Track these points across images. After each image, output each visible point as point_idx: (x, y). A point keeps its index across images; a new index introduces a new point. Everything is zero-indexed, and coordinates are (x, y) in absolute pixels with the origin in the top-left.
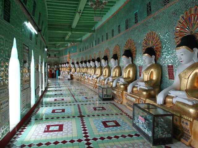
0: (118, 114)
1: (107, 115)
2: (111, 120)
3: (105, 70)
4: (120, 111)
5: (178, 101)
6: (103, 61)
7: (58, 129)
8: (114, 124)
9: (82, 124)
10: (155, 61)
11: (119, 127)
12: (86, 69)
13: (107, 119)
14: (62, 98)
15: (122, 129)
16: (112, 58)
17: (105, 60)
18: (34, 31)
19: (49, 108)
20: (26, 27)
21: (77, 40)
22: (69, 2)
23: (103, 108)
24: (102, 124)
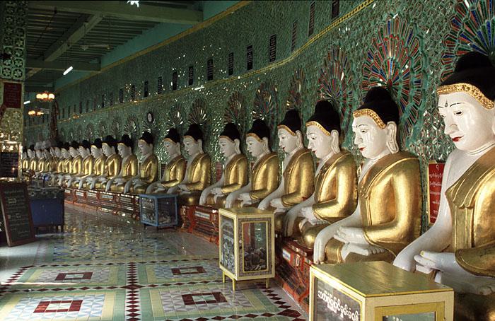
3: (233, 170)
6: (189, 142)
10: (399, 140)
16: (223, 134)
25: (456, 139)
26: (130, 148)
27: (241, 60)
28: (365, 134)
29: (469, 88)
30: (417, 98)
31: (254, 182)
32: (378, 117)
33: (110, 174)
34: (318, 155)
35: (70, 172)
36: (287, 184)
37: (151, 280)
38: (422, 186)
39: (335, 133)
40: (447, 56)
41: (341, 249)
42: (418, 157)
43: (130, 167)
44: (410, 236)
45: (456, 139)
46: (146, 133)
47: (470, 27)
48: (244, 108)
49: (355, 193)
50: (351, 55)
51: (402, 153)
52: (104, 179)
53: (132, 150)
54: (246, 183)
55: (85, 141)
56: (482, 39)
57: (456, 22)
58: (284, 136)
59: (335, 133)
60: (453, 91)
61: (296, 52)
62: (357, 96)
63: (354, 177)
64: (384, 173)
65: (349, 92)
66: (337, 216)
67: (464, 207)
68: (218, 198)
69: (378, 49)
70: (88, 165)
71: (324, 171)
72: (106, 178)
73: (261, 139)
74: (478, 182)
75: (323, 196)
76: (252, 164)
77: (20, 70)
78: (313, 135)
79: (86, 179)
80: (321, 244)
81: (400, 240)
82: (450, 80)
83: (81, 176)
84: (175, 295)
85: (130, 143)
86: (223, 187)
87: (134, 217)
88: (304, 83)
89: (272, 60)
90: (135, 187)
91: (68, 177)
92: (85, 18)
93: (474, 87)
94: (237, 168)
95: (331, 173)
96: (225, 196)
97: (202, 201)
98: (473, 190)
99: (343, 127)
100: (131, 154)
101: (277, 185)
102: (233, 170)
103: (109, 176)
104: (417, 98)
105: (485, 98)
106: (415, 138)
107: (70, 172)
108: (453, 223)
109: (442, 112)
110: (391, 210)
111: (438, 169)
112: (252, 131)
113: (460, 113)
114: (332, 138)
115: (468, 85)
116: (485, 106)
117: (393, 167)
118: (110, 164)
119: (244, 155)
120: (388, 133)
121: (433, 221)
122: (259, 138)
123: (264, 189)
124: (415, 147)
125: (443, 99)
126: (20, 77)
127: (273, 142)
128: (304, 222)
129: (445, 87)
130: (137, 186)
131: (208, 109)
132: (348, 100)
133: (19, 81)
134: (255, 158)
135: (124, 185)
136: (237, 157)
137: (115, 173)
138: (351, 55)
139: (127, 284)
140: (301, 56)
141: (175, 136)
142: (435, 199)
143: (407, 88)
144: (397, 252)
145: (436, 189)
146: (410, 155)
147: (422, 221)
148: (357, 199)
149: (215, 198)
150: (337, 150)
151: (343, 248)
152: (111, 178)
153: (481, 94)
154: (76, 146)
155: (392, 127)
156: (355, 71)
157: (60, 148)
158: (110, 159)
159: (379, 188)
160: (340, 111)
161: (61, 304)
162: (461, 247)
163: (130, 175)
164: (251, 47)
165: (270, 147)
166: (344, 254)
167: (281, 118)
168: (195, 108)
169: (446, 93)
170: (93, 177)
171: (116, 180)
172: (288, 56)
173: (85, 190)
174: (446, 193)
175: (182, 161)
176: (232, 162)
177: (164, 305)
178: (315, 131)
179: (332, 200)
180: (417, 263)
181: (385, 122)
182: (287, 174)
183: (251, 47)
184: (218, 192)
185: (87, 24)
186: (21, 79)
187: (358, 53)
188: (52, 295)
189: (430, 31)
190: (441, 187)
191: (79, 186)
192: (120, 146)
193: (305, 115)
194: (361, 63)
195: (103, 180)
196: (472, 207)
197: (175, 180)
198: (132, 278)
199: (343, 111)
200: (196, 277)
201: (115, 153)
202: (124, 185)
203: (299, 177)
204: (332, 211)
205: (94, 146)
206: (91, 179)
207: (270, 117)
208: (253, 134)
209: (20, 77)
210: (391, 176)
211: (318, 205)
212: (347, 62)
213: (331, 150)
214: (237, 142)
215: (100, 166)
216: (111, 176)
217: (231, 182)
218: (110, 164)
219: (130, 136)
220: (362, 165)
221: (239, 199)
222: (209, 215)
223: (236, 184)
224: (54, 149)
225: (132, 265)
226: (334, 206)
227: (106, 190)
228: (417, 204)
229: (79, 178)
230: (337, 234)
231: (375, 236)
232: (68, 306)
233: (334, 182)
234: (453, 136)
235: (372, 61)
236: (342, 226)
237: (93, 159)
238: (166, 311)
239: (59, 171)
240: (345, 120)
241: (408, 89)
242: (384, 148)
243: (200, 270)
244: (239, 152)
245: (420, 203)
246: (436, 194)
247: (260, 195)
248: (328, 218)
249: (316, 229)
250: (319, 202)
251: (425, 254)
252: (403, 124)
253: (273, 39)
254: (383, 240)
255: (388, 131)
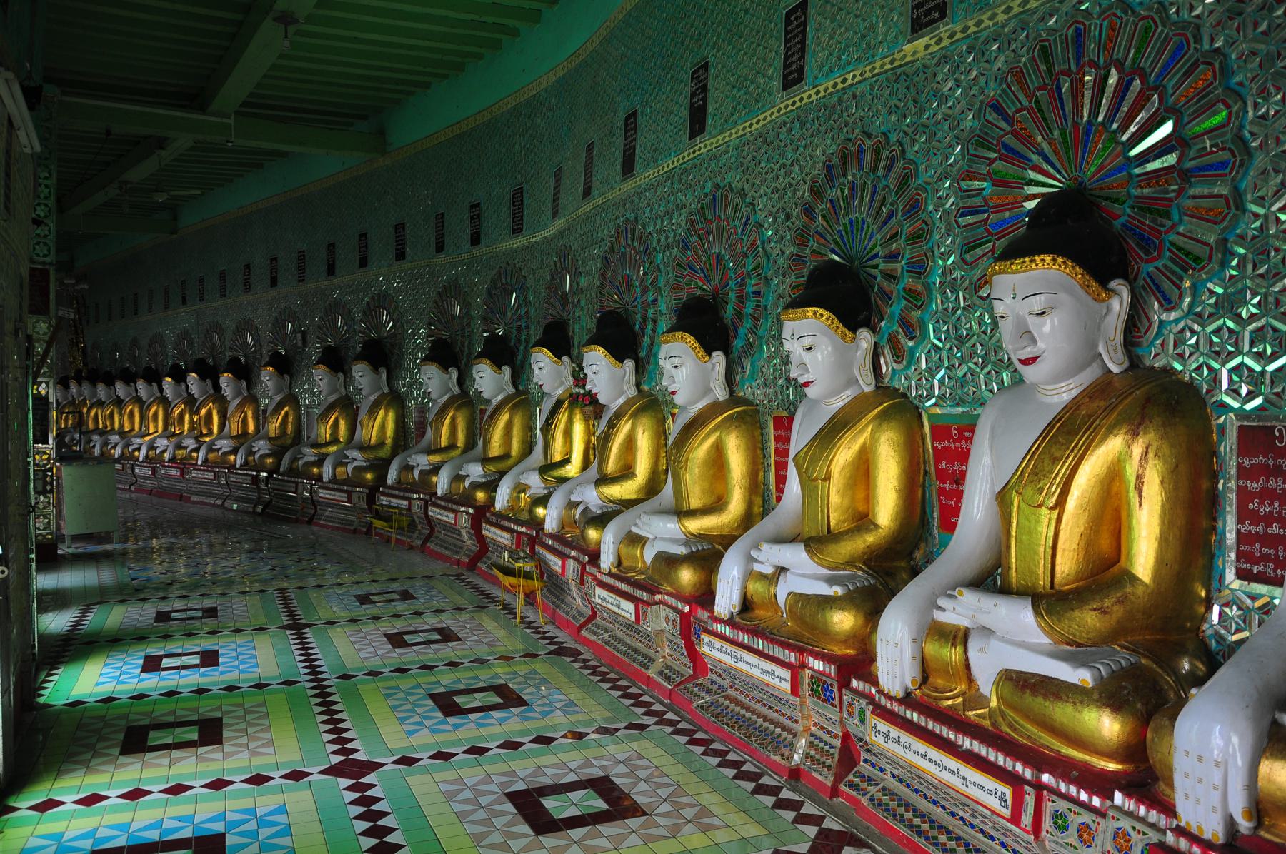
0: (535, 656)
1: (539, 740)
2: (481, 685)
3: (447, 421)
4: (628, 702)
5: (773, 513)
6: (361, 373)
7: (152, 734)
8: (600, 804)
9: (365, 825)
10: (730, 380)
11: (634, 823)
12: (342, 424)
13: (436, 651)
14: (207, 603)
15: (536, 715)
17: (375, 367)
18: (1083, 8)
19: (120, 687)
20: (1160, 561)
21: (1147, 387)
22: (408, 8)
23: (500, 690)
24: (509, 807)
25: (806, 384)
26: (244, 383)
27: (458, 226)
28: (679, 370)
29: (822, 315)
30: (756, 319)
31: (486, 443)
32: (697, 345)
33: (205, 432)
34: (602, 399)
35: (117, 426)
36: (547, 448)
37: (325, 614)
38: (764, 449)
39: (629, 365)
40: (797, 260)
41: (643, 548)
42: (757, 405)
43: (245, 417)
44: (747, 521)
45: (806, 384)
46: (276, 355)
47: (827, 221)
48: (466, 314)
49: (663, 461)
50: (656, 239)
51: (734, 400)
52: (192, 441)
53: (249, 388)
54: (470, 445)
55: (148, 368)
56: (841, 249)
57: (809, 212)
58: (541, 365)
59: (629, 365)
60: (801, 318)
61: (560, 223)
62: (666, 307)
63: (660, 434)
64: (707, 430)
65: (651, 299)
66: (634, 497)
67: (816, 479)
68: (421, 472)
69: (698, 235)
70: (156, 414)
71: (612, 425)
72: (196, 438)
73: (500, 368)
74: (835, 445)
75: (611, 466)
76: (483, 412)
77: (45, 244)
78: (594, 368)
79: (153, 441)
80: (612, 540)
81: (732, 529)
82: (799, 303)
83: (143, 436)
84: (374, 634)
85: (245, 373)
86: (429, 452)
87: (259, 509)
88: (576, 275)
89: (517, 230)
90: (257, 456)
91: (114, 438)
92: (161, 143)
93: (829, 314)
94: (453, 419)
95: (625, 428)
96: (436, 469)
97: (392, 477)
98: (828, 456)
99: (642, 354)
100: (245, 394)
101: (528, 448)
102: (447, 421)
103: (202, 435)
104: (756, 319)
105: (844, 329)
106: (753, 377)
107: (117, 426)
108: (804, 502)
109: (787, 345)
110: (153, 637)
111: (784, 425)
112: (481, 355)
113: (810, 348)
114: (625, 371)
115: (821, 311)
116: (843, 339)
117: (722, 420)
118: (203, 412)
119: (465, 398)
120: (713, 369)
121: (779, 499)
122: (495, 368)
123: (506, 456)
124: (751, 390)
125: (789, 328)
126: (45, 256)
127: (520, 373)
128: (580, 508)
129: (791, 311)
130: (262, 452)
131: (397, 312)
132: (651, 311)
133: (44, 263)
134: (488, 402)
135: (235, 451)
136: (453, 399)
137: (215, 429)
138: (656, 239)
139: (286, 623)
140: (570, 229)
141: (335, 361)
142: (782, 467)
143: (741, 299)
144: (727, 547)
145: (782, 453)
146: (744, 401)
147: (764, 501)
148: (667, 470)
149: (416, 473)
150: (632, 392)
151: (647, 545)
152: (207, 439)
153: (837, 322)
154: (129, 379)
155: (719, 358)
156: (661, 266)
157: (94, 383)
158: (203, 404)
159: (700, 450)
160: (637, 327)
161: (183, 658)
162: (814, 534)
163: (245, 434)
164: (478, 205)
165: (515, 382)
166: (649, 554)
167: (536, 333)
168: (371, 312)
169: (792, 320)
170: (168, 438)
171: (219, 444)
172: (546, 226)
173: (154, 462)
174: (794, 459)
175: (347, 406)
176: (444, 409)
177: (360, 650)
178: (598, 362)
179: (626, 472)
180: (756, 561)
181: (709, 352)
182: (548, 428)
183: (478, 205)
184: (422, 461)
185: (163, 153)
186: (48, 260)
187: (667, 238)
188: (180, 643)
189: (775, 220)
190: (788, 449)
191: (142, 454)
192: (225, 380)
193: (577, 330)
194: (671, 254)
195: (191, 443)
196: (827, 478)
197: (335, 440)
198: (291, 613)
199: (643, 330)
200: (400, 607)
201: (212, 392)
202: (235, 451)
203: (568, 433)
204: (618, 491)
205: (169, 379)
206: (165, 442)
207: (514, 330)
208: (484, 360)
209: (45, 256)
210: (718, 434)
211: (603, 480)
212: (648, 252)
213: (622, 392)
214: (454, 373)
215: (181, 416)
216: (206, 435)
217: (444, 443)
218: (203, 412)
219: (243, 360)
220: (673, 416)
221: (460, 473)
222: (406, 503)
223: (452, 446)
224: (80, 384)
225: (282, 590)
226: (630, 482)
227: (200, 463)
228: (757, 476)
229: (139, 440)
230: (636, 525)
231: (694, 525)
232: (196, 660)
233: (630, 444)
234: (801, 380)
235: (689, 253)
236: (645, 513)
237: (164, 401)
238: (365, 658)
239: (91, 426)
240: (647, 340)
241: (743, 303)
242: (708, 390)
243: (406, 595)
244: (457, 390)
245: (761, 474)
246: (783, 460)
247: (502, 466)
248: (620, 500)
249: (601, 520)
250: (606, 475)
251: (765, 547)
252: (735, 354)
253: (518, 198)
254: (706, 530)
255: (714, 365)
